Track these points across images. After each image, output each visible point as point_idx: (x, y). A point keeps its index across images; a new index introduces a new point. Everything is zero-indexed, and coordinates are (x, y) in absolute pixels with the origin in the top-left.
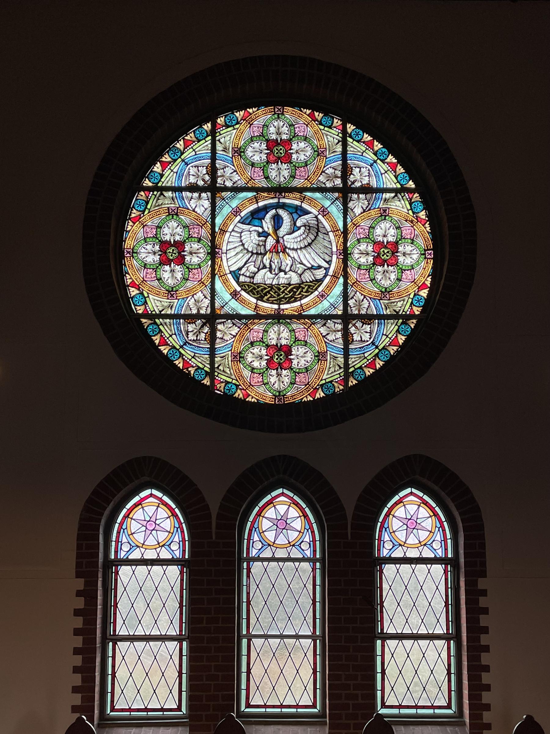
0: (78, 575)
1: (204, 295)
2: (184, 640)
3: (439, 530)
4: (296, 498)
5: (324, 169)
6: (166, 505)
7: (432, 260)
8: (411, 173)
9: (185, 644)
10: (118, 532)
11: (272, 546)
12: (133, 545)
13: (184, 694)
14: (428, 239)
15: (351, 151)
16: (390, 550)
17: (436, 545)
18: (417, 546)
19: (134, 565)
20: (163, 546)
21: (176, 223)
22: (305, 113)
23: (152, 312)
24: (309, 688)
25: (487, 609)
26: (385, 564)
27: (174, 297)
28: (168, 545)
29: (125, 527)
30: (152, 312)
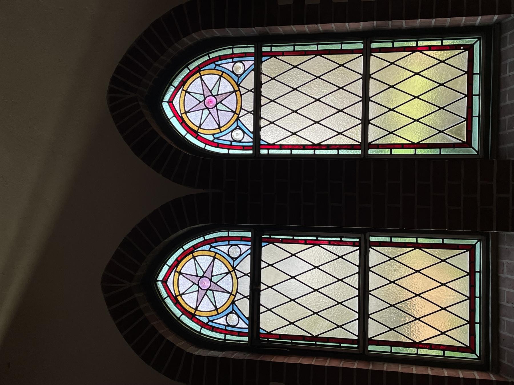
2: (367, 240)
4: (176, 83)
6: (178, 262)
9: (373, 239)
10: (218, 146)
12: (235, 125)
16: (244, 132)
17: (235, 252)
18: (239, 96)
19: (259, 309)
26: (259, 328)
29: (212, 136)
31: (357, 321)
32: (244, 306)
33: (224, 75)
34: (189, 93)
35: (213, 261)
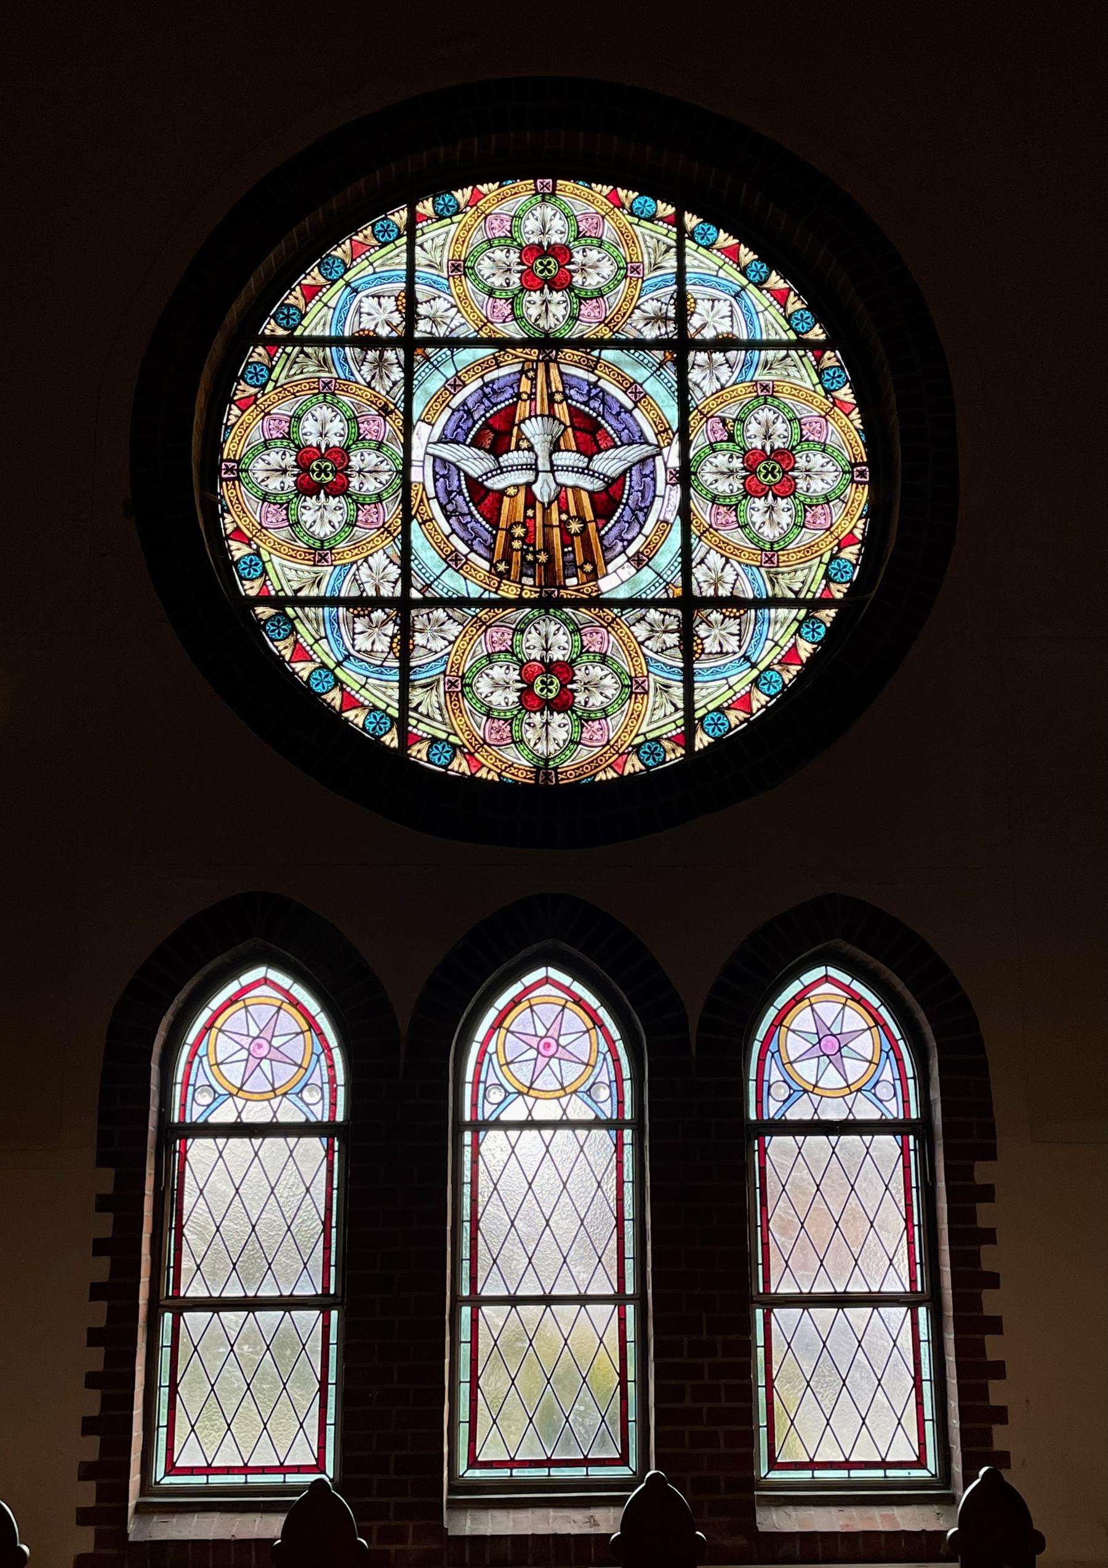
0: (102, 1162)
1: (388, 557)
2: (333, 1306)
3: (888, 1057)
5: (639, 303)
7: (867, 486)
8: (819, 310)
9: (334, 1314)
11: (812, 1092)
13: (330, 1431)
14: (856, 442)
15: (694, 266)
16: (499, 1104)
17: (884, 1091)
18: (558, 1094)
20: (285, 1094)
21: (330, 409)
22: (600, 193)
23: (277, 592)
24: (610, 1418)
25: (992, 1232)
26: (194, 1137)
27: (327, 561)
28: (297, 1094)
30: (277, 592)
31: (208, 1295)
32: (800, 1112)
33: (302, 1071)
34: (562, 1010)
35: (295, 1064)
